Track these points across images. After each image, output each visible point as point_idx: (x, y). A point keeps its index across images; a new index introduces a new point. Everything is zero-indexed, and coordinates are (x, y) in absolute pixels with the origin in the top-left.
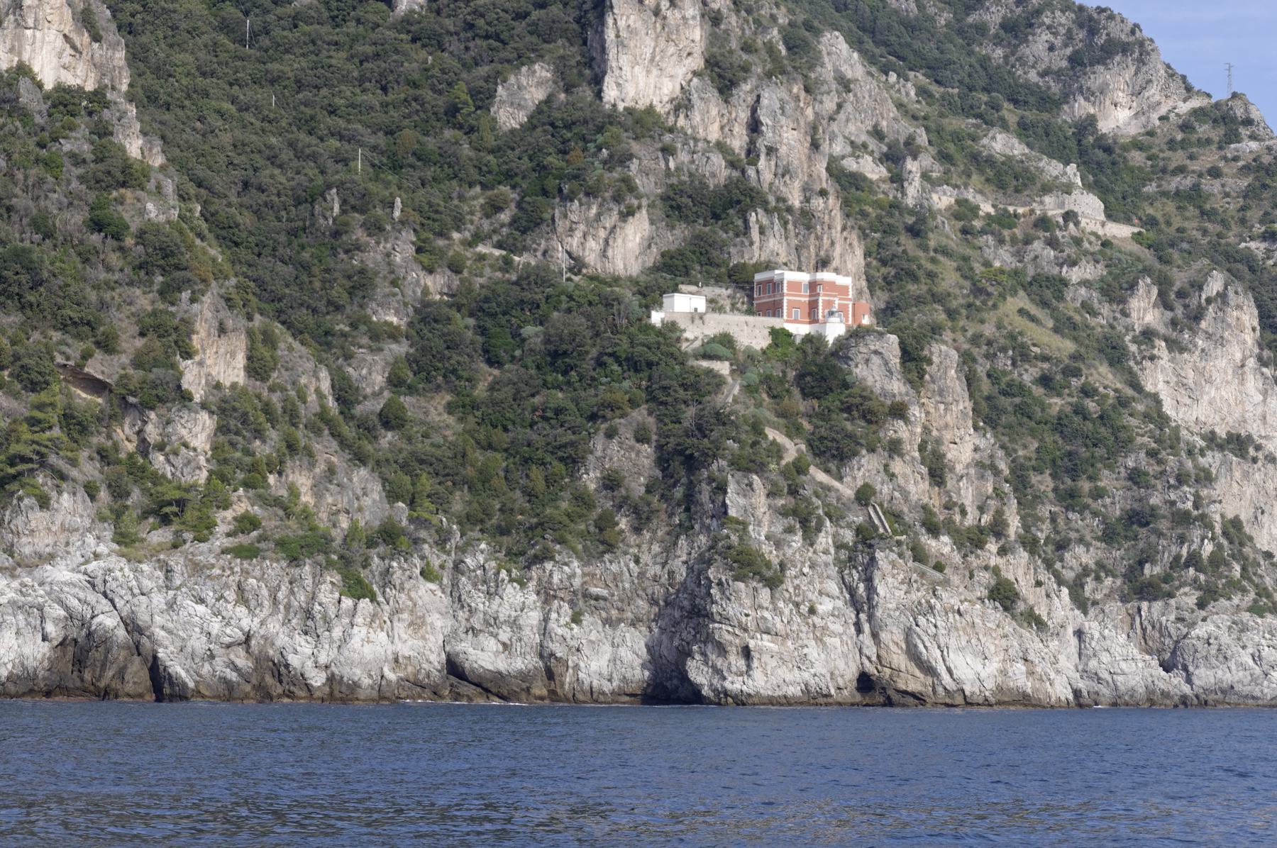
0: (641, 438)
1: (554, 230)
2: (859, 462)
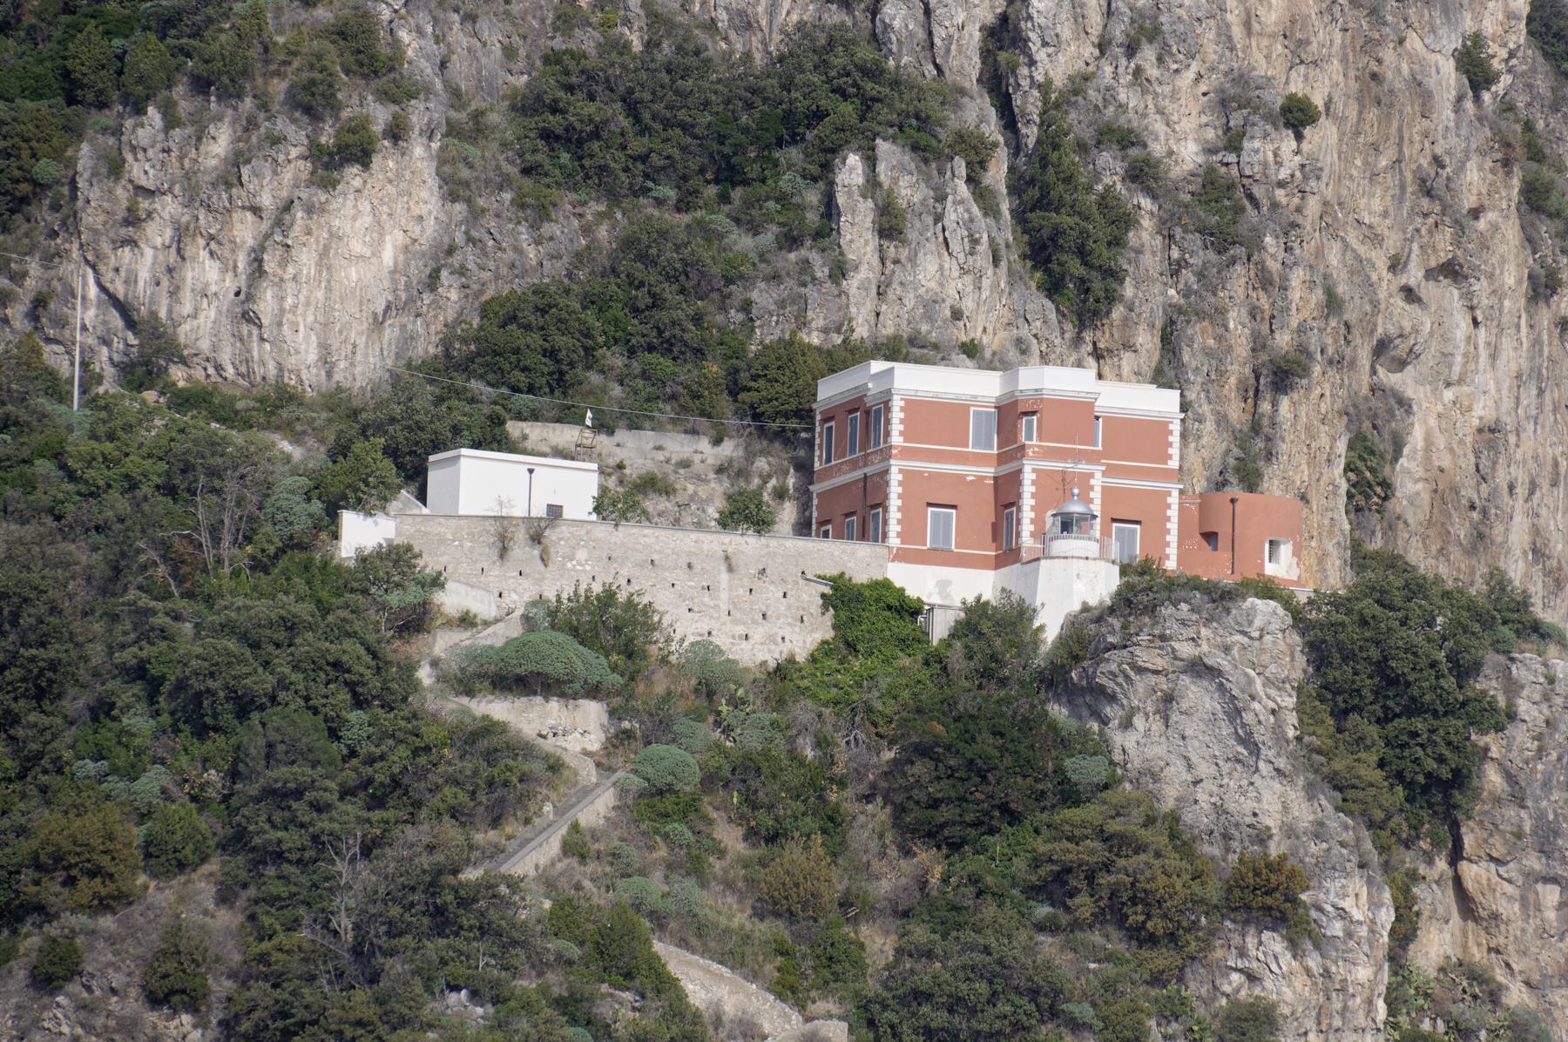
1: (71, 223)
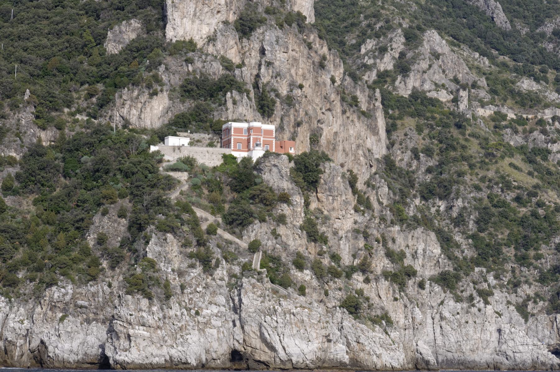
0: (122, 215)
1: (115, 105)
2: (252, 227)
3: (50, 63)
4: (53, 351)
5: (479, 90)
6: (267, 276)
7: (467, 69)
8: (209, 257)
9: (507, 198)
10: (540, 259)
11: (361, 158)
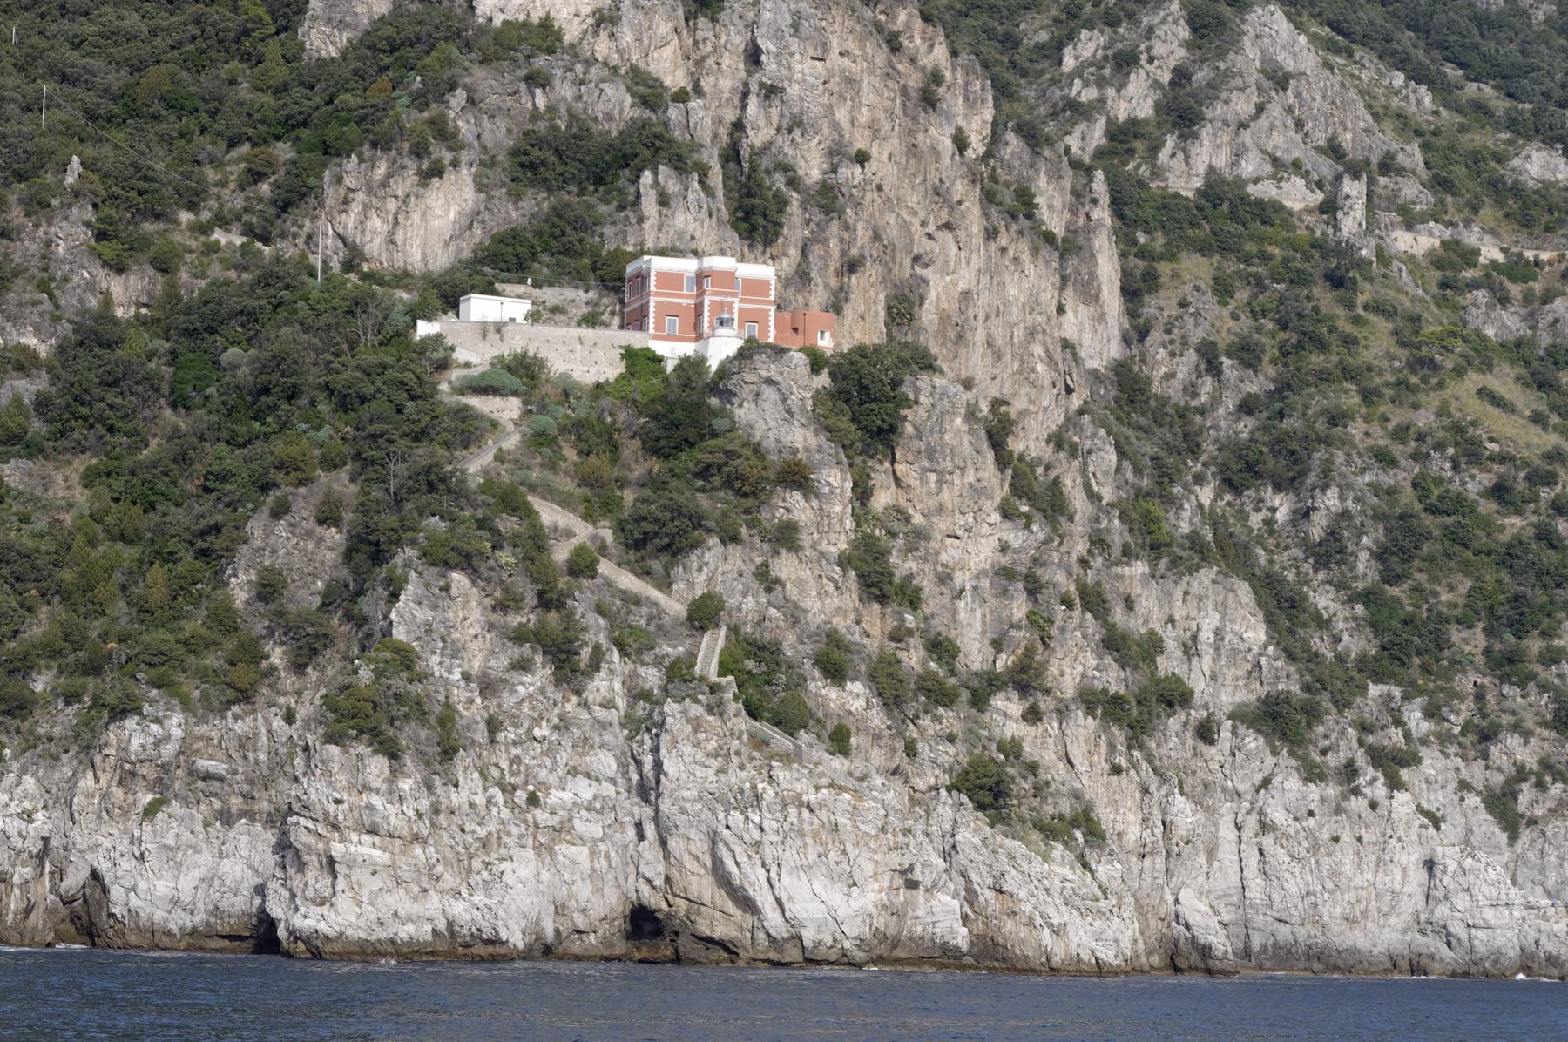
1: (321, 204)
2: (700, 557)
3: (143, 81)
4: (122, 900)
5: (1400, 179)
6: (736, 698)
7: (1369, 117)
8: (570, 642)
9: (1469, 487)
10: (1558, 663)
11: (1040, 367)
